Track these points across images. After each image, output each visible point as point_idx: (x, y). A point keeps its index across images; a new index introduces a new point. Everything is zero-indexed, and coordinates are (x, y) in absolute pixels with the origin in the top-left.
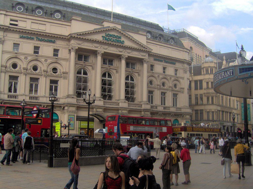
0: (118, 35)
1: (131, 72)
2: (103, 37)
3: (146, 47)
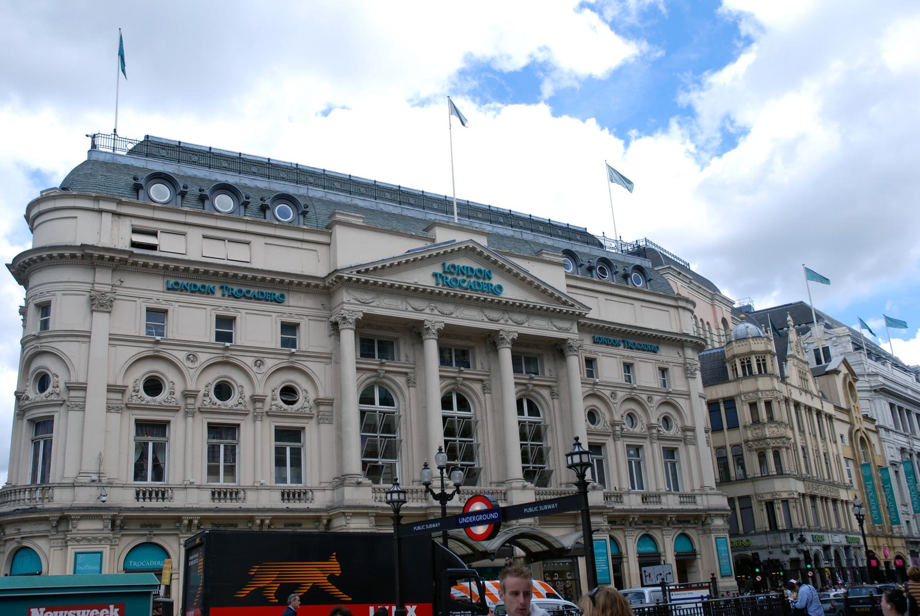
0: (483, 269)
1: (531, 387)
2: (435, 275)
3: (570, 302)
